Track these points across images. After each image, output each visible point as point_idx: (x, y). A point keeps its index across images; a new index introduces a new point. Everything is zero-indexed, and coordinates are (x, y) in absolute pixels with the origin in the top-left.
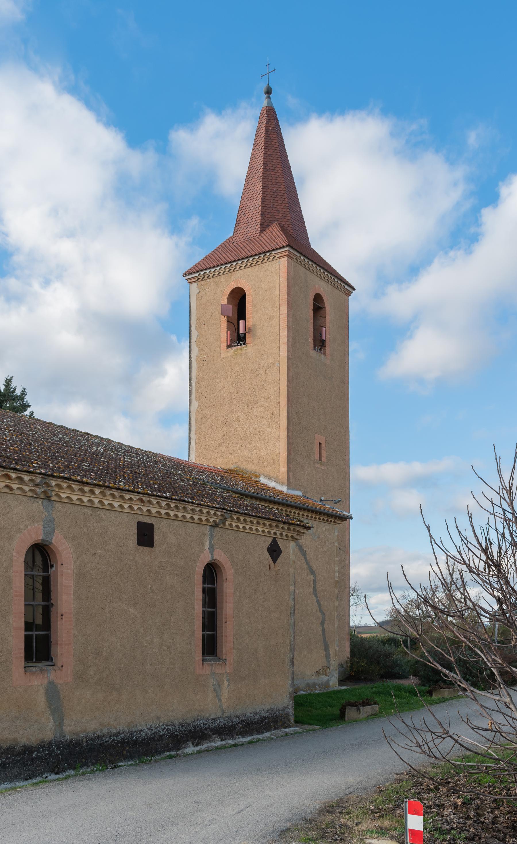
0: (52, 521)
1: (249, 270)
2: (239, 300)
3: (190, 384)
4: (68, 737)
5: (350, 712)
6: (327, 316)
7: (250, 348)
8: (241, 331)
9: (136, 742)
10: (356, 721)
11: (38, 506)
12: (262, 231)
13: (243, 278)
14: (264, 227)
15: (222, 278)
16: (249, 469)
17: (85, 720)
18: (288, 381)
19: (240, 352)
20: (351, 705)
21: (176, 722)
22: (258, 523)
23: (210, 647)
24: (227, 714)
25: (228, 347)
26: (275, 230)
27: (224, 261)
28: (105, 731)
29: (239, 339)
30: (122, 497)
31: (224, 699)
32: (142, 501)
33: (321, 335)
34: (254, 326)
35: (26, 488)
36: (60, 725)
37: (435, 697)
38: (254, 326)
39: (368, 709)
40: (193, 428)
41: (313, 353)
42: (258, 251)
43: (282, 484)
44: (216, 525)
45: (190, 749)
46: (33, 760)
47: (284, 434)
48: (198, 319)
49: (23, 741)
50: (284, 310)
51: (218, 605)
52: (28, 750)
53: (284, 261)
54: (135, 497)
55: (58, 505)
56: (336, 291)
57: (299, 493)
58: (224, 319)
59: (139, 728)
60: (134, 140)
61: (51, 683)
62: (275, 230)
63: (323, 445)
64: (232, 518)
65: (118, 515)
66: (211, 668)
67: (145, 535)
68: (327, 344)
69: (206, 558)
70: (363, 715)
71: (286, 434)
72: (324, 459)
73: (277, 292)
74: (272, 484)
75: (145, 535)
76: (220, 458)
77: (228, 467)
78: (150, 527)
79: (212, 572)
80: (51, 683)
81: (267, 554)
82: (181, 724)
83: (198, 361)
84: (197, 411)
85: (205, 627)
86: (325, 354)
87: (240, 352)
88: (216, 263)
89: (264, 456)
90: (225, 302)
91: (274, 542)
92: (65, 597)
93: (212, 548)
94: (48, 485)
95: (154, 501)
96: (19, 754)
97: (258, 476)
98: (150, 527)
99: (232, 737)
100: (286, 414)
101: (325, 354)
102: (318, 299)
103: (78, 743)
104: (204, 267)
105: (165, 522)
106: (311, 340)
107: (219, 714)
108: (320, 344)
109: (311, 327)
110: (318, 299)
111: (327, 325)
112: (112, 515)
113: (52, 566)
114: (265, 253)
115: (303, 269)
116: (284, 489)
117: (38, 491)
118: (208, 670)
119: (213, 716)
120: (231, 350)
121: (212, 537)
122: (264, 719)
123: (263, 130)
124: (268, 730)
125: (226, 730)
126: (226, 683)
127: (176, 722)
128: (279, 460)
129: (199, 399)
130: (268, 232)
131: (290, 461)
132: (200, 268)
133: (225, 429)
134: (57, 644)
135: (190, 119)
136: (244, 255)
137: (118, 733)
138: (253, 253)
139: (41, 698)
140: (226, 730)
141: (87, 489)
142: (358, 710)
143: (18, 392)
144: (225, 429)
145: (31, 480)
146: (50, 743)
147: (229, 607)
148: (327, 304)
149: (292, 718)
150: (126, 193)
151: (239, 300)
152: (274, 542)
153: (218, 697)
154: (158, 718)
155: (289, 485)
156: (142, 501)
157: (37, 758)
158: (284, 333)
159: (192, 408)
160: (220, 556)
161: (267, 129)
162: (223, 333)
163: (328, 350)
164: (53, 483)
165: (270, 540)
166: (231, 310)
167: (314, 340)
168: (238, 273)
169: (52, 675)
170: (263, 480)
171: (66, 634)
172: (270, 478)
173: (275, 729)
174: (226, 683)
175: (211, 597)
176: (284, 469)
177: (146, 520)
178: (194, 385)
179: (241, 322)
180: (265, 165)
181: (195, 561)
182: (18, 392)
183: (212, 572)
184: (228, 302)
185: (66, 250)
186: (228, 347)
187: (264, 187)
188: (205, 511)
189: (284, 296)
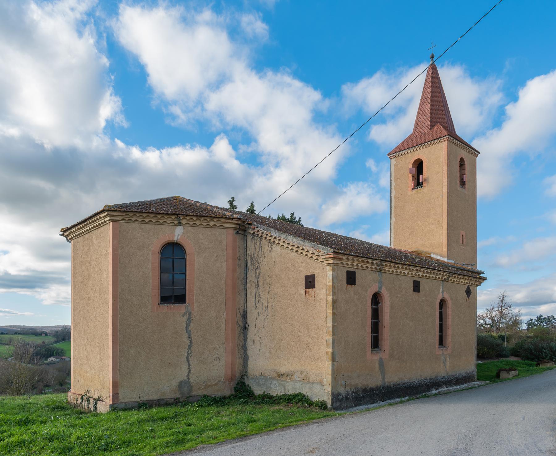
0: (381, 282)
1: (424, 150)
2: (419, 166)
3: (391, 209)
4: (387, 384)
5: (503, 375)
6: (466, 169)
7: (425, 189)
8: (421, 181)
9: (412, 387)
10: (505, 380)
11: (376, 275)
12: (431, 129)
13: (421, 153)
14: (432, 126)
15: (409, 155)
16: (425, 250)
17: (395, 376)
18: (448, 204)
19: (419, 191)
20: (505, 370)
21: (428, 378)
22: (463, 278)
23: (441, 341)
24: (449, 374)
25: (413, 189)
26: (439, 127)
27: (410, 146)
28: (400, 382)
29: (418, 184)
30: (409, 269)
31: (447, 367)
32: (417, 270)
33: (463, 179)
34: (428, 178)
35: (374, 267)
36: (384, 378)
37: (541, 367)
38: (428, 178)
39: (513, 373)
40: (392, 232)
41: (460, 189)
42: (430, 139)
43: (444, 257)
44: (445, 280)
45: (434, 392)
46: (374, 394)
47: (445, 232)
48: (395, 176)
49: (370, 386)
50: (445, 168)
51: (444, 320)
52: (372, 389)
53: (446, 143)
54: (415, 268)
55: (384, 274)
56: (471, 155)
57: (453, 262)
58: (410, 175)
59: (414, 380)
60: (326, 95)
61: (381, 358)
62: (439, 127)
63: (464, 236)
64: (452, 276)
65: (405, 277)
66: (440, 352)
67: (417, 287)
68: (466, 183)
69: (440, 297)
70: (511, 376)
71: (446, 231)
72: (464, 243)
73: (441, 159)
74: (438, 258)
75: (417, 287)
76: (407, 245)
77: (413, 250)
78: (418, 282)
79: (442, 302)
80: (381, 358)
81: (465, 294)
82: (430, 379)
83: (395, 197)
84: (395, 223)
85: (439, 332)
86: (465, 188)
87: (419, 191)
88: (406, 148)
89: (434, 242)
90: (411, 166)
91: (468, 288)
92: (386, 318)
93: (443, 292)
94: (382, 265)
95: (422, 270)
96: (369, 392)
97: (430, 254)
98: (418, 282)
99: (451, 386)
100: (446, 221)
101: (465, 188)
102: (462, 160)
103: (390, 387)
104: (399, 150)
105: (424, 280)
106: (458, 182)
107: (446, 374)
108: (463, 183)
109: (459, 176)
110: (462, 160)
111: (466, 173)
112: (403, 278)
113: (379, 303)
114: (435, 140)
115: (454, 146)
116: (445, 260)
117: (378, 268)
118: (441, 352)
119: (443, 375)
120: (414, 191)
121: (443, 286)
122: (464, 377)
123: (430, 77)
124: (466, 382)
125: (449, 382)
126: (448, 359)
127: (428, 378)
128: (442, 245)
129: (395, 216)
130: (435, 129)
131: (449, 245)
132: (397, 151)
133: (410, 231)
134: (382, 340)
135: (355, 79)
136: (422, 142)
137: (405, 383)
138: (427, 141)
139: (377, 365)
140: (449, 382)
141: (396, 266)
142: (508, 373)
143: (297, 219)
144: (410, 231)
145: (376, 263)
146: (380, 387)
147: (450, 321)
148: (466, 163)
149: (476, 377)
150: (320, 119)
151: (419, 166)
152: (468, 288)
153: (445, 365)
154: (421, 376)
155: (448, 258)
156: (417, 270)
157: (376, 394)
158: (445, 180)
159: (392, 222)
160: (446, 296)
161: (432, 77)
162: (409, 181)
163: (466, 186)
164: (384, 264)
165: (466, 286)
166: (414, 171)
167: (460, 182)
168: (418, 152)
169: (381, 355)
170: (433, 256)
171: (386, 334)
172: (437, 255)
173: (469, 382)
174: (448, 359)
175: (376, 314)
176: (445, 250)
177: (417, 279)
178: (393, 210)
179: (421, 176)
180: (432, 95)
181: (436, 299)
182: (297, 219)
183: (442, 302)
184: (413, 167)
185: (286, 150)
186: (413, 189)
187: (432, 106)
188: (442, 273)
189: (446, 161)
